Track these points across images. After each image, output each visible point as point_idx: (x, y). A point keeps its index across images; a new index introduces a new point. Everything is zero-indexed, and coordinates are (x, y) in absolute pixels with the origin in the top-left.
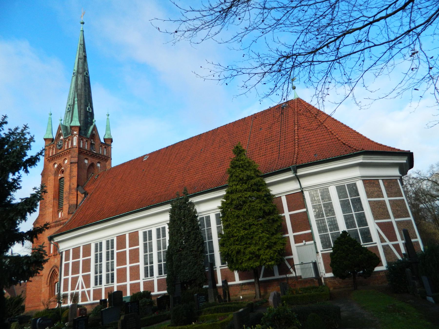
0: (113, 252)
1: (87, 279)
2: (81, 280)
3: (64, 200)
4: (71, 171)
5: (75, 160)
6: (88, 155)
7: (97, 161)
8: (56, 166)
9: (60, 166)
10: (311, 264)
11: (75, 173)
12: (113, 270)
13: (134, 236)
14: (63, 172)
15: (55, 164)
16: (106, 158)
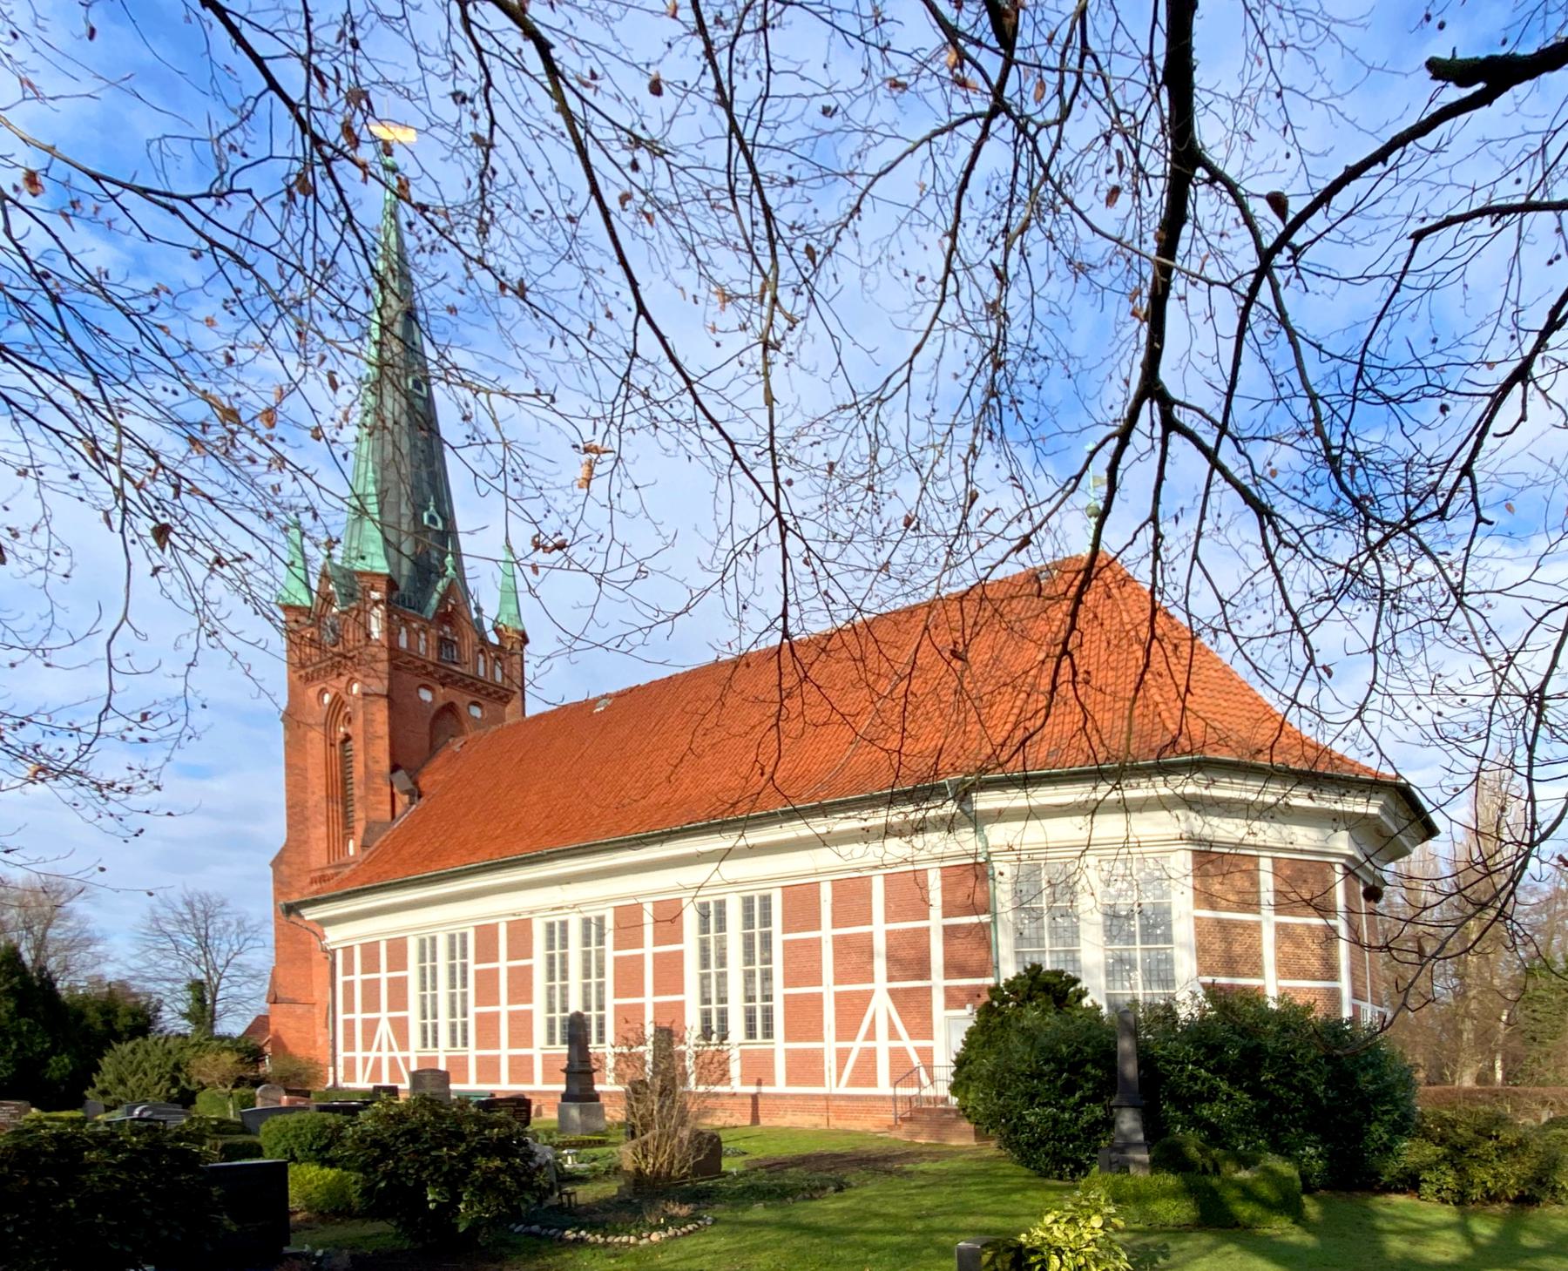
0: (464, 966)
1: (400, 1027)
2: (384, 1029)
3: (357, 806)
4: (368, 722)
5: (381, 686)
6: (429, 674)
7: (470, 699)
8: (327, 698)
9: (338, 703)
10: (750, 1101)
11: (382, 726)
12: (465, 1015)
13: (520, 931)
14: (349, 720)
15: (322, 692)
16: (502, 693)
